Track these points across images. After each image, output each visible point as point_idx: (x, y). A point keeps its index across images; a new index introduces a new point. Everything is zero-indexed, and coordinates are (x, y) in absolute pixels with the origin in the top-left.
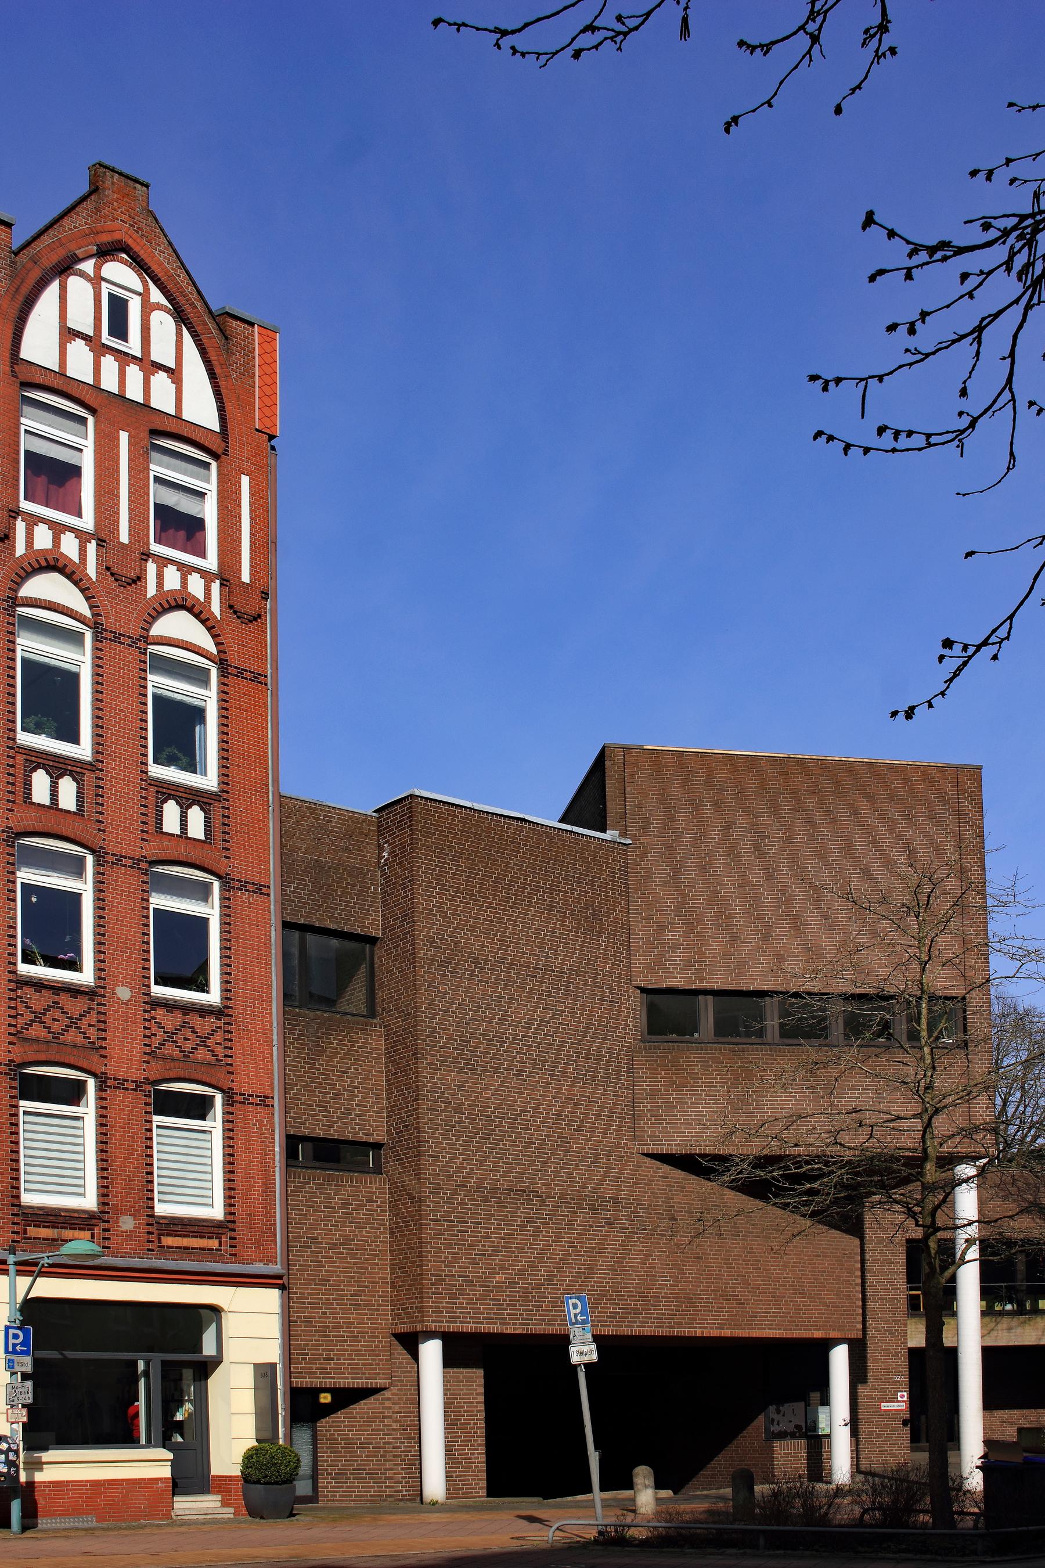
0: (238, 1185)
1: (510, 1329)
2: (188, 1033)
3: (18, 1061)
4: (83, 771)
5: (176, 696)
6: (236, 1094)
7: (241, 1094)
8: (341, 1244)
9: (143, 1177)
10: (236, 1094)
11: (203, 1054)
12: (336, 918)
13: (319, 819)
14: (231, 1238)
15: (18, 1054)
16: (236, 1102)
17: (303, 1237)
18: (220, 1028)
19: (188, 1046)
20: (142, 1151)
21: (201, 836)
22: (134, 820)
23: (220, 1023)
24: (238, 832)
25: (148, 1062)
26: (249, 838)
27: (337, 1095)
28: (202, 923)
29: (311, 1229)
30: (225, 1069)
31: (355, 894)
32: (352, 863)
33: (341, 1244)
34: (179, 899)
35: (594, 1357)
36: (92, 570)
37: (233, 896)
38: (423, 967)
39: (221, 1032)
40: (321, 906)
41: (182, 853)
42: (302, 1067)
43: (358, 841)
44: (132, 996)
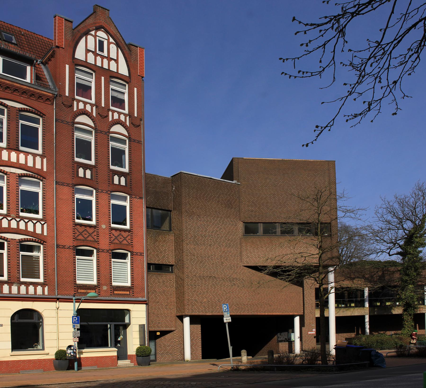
1: (208, 314)
2: (121, 237)
3: (76, 245)
11: (125, 242)
19: (121, 240)
23: (129, 234)
27: (161, 252)
35: (230, 321)
36: (94, 114)
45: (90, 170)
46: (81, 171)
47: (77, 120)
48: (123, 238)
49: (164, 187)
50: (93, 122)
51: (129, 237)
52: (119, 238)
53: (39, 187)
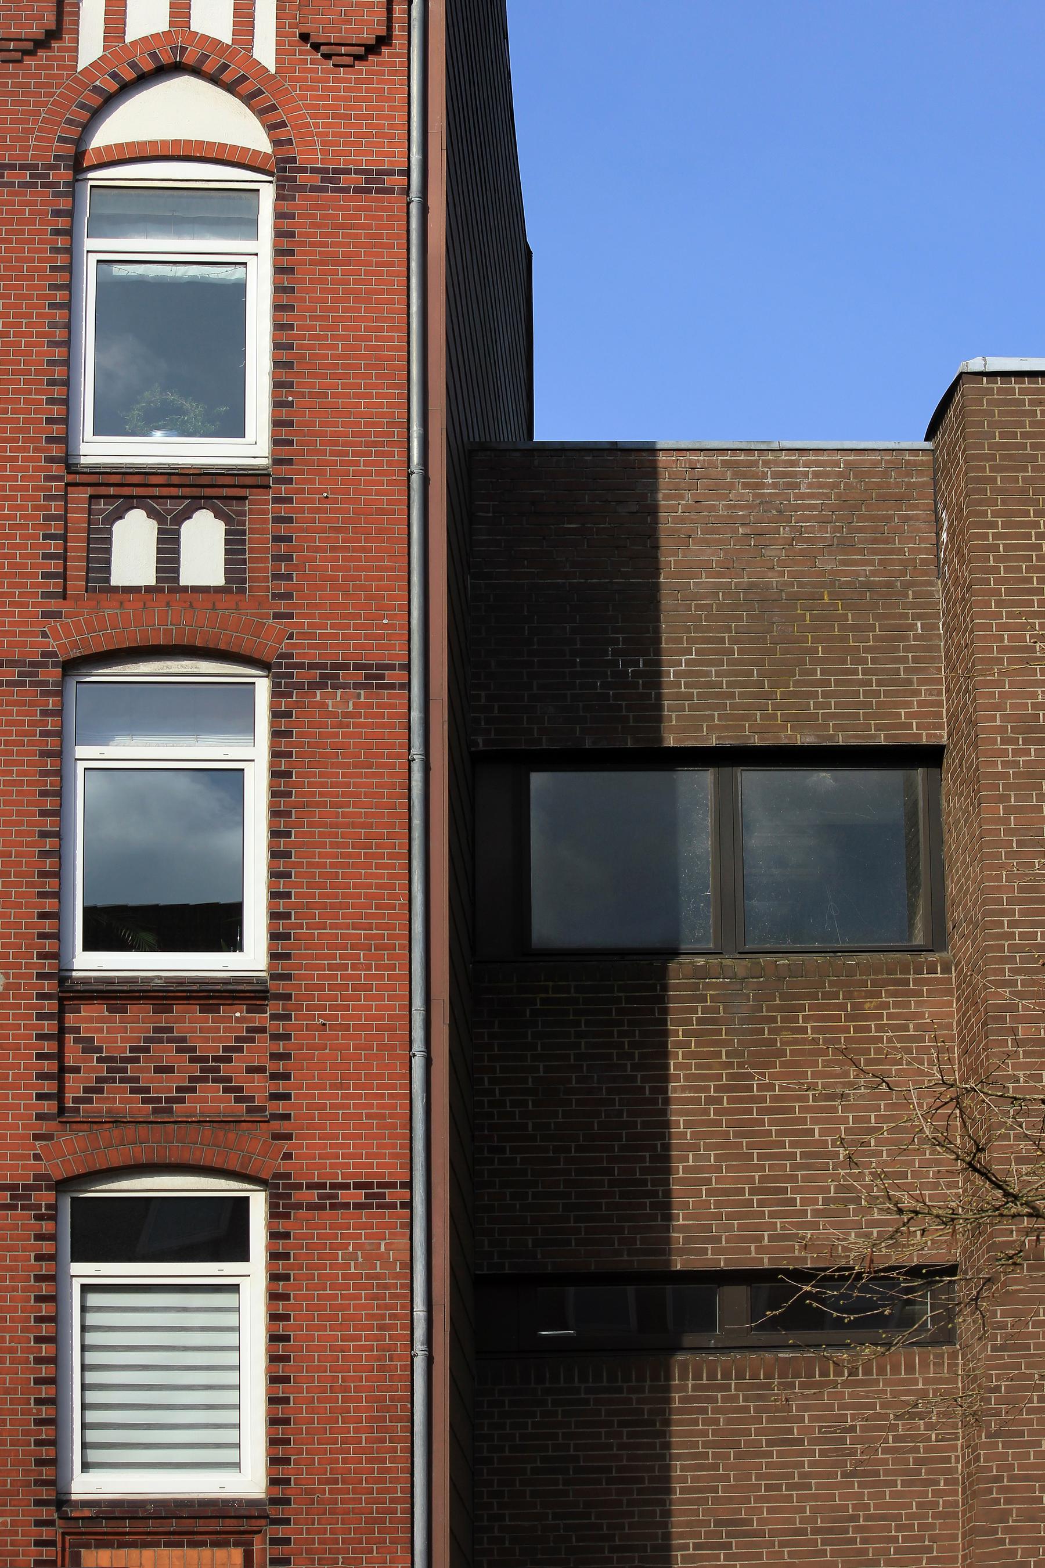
0: (299, 1409)
2: (168, 1054)
3: (61, 1173)
4: (240, 492)
5: (180, 271)
6: (298, 1186)
7: (310, 1186)
8: (816, 1531)
9: (29, 1412)
10: (298, 1186)
11: (210, 1100)
13: (763, 486)
14: (274, 1541)
15: (69, 1151)
16: (299, 1206)
17: (706, 1523)
19: (166, 1085)
20: (28, 1350)
21: (216, 577)
23: (258, 1019)
25: (48, 1137)
27: (816, 1157)
29: (730, 1500)
30: (263, 1133)
32: (857, 574)
33: (816, 1531)
34: (190, 739)
36: (265, 50)
38: (1005, 798)
39: (263, 1042)
40: (768, 696)
42: (710, 1100)
43: (872, 518)
45: (152, 514)
46: (133, 549)
47: (109, 133)
48: (185, 1068)
49: (846, 545)
50: (261, 113)
53: (250, 729)
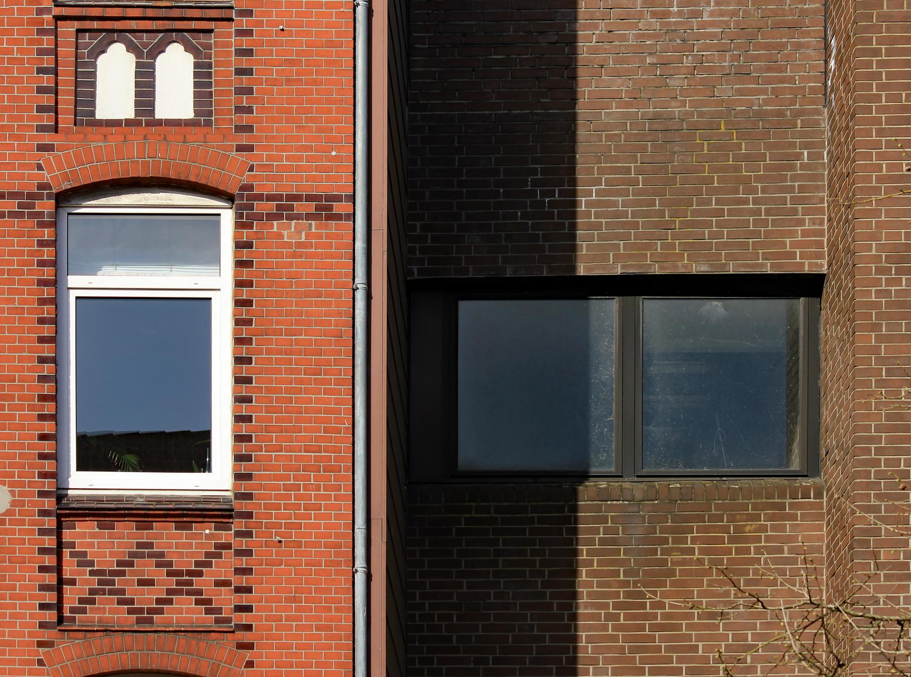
2: (147, 568)
11: (184, 611)
12: (709, 246)
13: (667, 14)
18: (228, 546)
19: (146, 597)
22: (21, 109)
23: (226, 536)
24: (274, 82)
26: (300, 92)
28: (198, 308)
31: (758, 179)
32: (751, 104)
34: (165, 270)
37: (259, 236)
38: (876, 327)
41: (135, 159)
42: (609, 617)
43: (768, 47)
44: (14, 503)
48: (164, 582)
49: (743, 74)
51: (224, 567)
52: (128, 583)
